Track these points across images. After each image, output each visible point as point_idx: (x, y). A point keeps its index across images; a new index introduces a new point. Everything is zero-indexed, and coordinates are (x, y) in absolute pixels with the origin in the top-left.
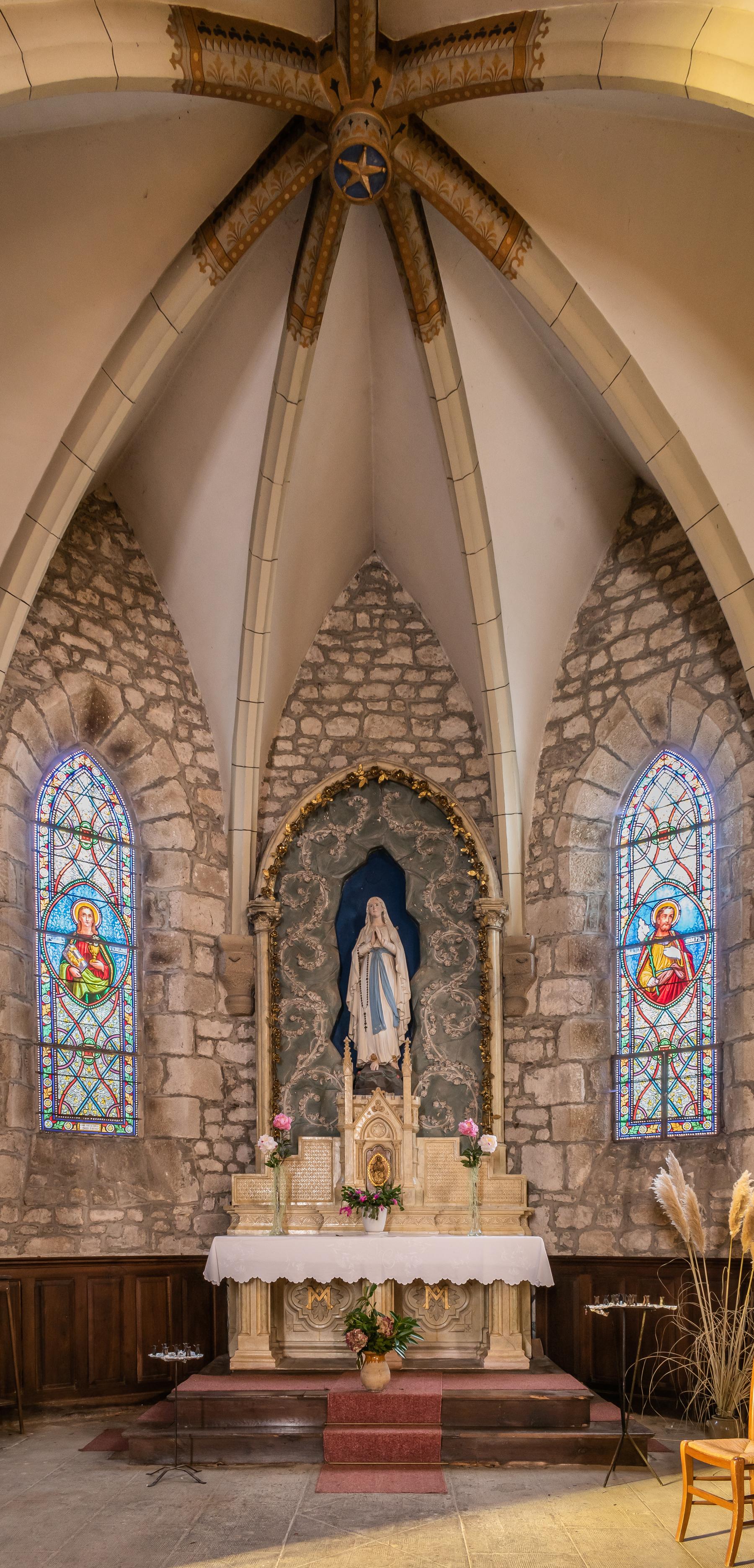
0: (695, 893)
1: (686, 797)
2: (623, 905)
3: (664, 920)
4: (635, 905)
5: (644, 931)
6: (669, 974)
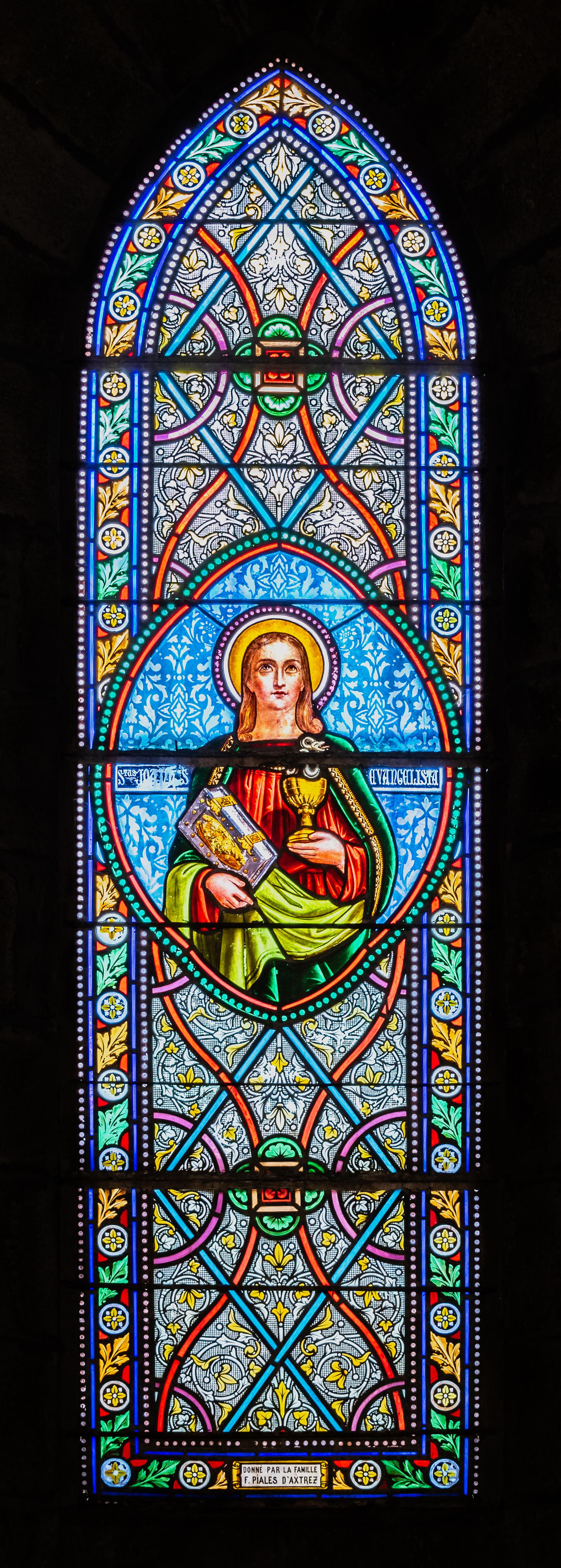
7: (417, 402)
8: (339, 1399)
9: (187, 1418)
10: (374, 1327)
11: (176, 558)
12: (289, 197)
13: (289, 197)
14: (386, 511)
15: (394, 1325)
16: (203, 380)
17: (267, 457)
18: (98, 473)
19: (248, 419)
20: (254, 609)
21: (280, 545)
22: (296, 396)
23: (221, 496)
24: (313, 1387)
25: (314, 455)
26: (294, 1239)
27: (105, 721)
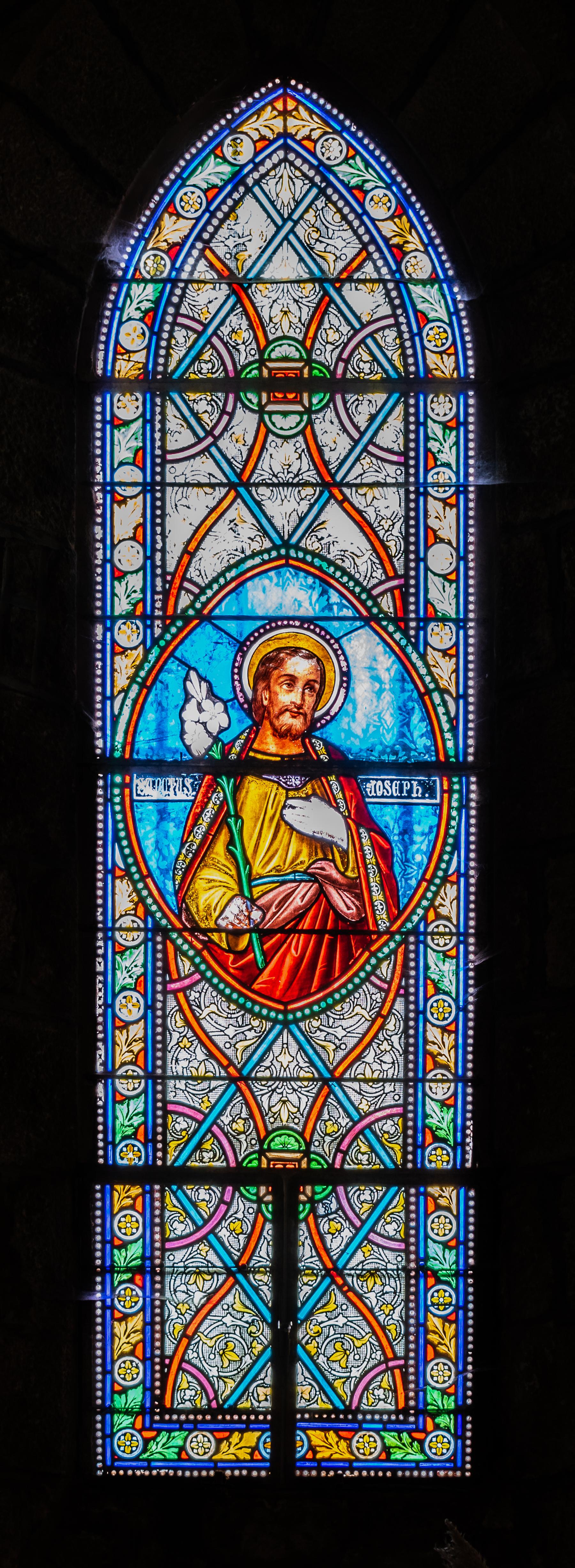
0: (400, 620)
1: (369, 270)
2: (122, 606)
3: (287, 697)
4: (173, 614)
5: (203, 723)
6: (302, 895)
7: (415, 425)
8: (341, 1378)
9: (193, 1393)
10: (376, 1309)
11: (383, 994)
12: (293, 220)
13: (293, 220)
14: (386, 528)
15: (394, 1309)
16: (212, 400)
17: (274, 475)
18: (113, 492)
19: (314, 1129)
20: (263, 627)
21: (287, 562)
22: (269, 1150)
23: (341, 1054)
24: (317, 1365)
25: (319, 473)
26: (271, 337)
27: (450, 841)
